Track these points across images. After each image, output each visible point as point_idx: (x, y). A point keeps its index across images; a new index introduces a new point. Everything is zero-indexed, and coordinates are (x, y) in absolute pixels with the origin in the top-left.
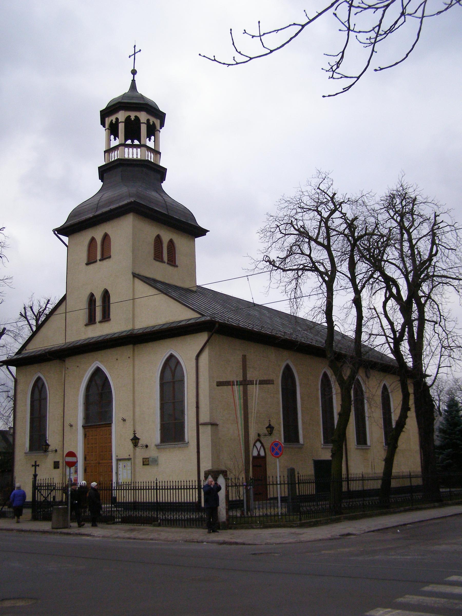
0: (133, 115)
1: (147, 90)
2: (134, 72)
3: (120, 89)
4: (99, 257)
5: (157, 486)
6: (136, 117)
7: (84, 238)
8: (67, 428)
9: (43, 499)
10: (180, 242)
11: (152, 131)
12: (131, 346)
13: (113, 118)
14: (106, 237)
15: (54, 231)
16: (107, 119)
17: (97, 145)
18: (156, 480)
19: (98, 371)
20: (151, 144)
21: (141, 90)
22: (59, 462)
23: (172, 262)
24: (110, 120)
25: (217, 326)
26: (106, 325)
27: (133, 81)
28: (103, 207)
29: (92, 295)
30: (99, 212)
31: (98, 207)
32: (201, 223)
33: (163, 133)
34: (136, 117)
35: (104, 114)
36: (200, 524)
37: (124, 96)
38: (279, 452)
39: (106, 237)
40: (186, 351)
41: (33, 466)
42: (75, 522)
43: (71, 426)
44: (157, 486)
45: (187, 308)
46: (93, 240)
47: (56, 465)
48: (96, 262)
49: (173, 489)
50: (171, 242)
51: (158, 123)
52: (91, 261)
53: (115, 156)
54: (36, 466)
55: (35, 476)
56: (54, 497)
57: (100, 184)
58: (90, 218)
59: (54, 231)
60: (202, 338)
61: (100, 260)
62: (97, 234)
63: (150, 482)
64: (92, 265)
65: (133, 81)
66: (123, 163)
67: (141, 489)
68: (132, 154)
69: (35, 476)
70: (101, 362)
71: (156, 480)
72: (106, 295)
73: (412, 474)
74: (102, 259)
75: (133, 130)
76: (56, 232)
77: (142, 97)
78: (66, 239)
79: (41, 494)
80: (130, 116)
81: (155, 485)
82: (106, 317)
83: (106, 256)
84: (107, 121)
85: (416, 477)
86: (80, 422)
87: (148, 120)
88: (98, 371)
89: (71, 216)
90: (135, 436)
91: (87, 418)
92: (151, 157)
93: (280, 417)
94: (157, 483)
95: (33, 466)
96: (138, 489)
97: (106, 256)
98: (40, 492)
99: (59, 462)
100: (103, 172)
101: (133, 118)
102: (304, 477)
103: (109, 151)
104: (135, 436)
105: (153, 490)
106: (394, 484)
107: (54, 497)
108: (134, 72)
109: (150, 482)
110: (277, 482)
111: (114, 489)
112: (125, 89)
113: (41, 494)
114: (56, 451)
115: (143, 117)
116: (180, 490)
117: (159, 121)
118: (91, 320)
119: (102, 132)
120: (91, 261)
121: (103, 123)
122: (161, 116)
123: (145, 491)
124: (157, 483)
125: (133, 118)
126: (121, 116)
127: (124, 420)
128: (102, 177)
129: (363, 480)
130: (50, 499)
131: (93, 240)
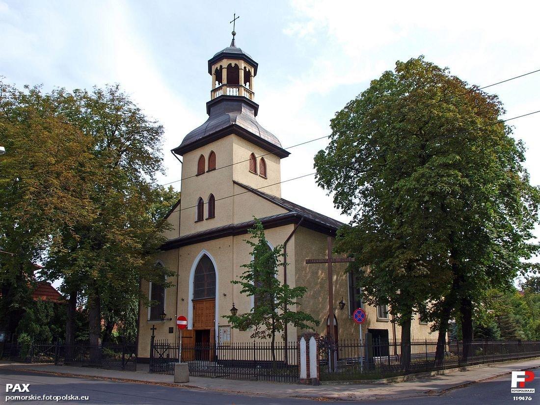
0: (233, 63)
1: (243, 46)
2: (234, 34)
3: (223, 45)
4: (206, 169)
5: (255, 347)
7: (196, 155)
8: (179, 302)
9: (159, 356)
10: (270, 162)
11: (248, 78)
12: (232, 236)
13: (218, 66)
14: (212, 154)
15: (172, 151)
16: (213, 67)
17: (204, 87)
19: (205, 258)
20: (247, 87)
21: (238, 45)
22: (173, 328)
23: (264, 175)
24: (215, 68)
25: (302, 219)
26: (212, 221)
27: (233, 39)
28: (210, 130)
29: (201, 199)
30: (207, 134)
31: (206, 131)
32: (284, 147)
33: (254, 80)
35: (211, 63)
36: (294, 380)
37: (226, 49)
38: (361, 318)
39: (212, 154)
40: (275, 238)
41: (151, 329)
43: (183, 300)
44: (255, 347)
45: (275, 205)
46: (202, 157)
47: (171, 330)
48: (204, 173)
49: (234, 349)
50: (263, 160)
52: (201, 172)
53: (219, 94)
54: (153, 329)
55: (153, 337)
56: (168, 355)
57: (207, 117)
58: (200, 140)
59: (172, 151)
60: (291, 228)
61: (207, 172)
62: (205, 151)
64: (201, 176)
65: (233, 39)
66: (225, 98)
68: (232, 92)
69: (153, 337)
70: (208, 250)
72: (212, 199)
73: (428, 341)
75: (233, 81)
76: (173, 152)
78: (181, 158)
79: (158, 352)
80: (231, 64)
82: (212, 215)
83: (212, 168)
84: (214, 68)
85: (432, 344)
86: (191, 296)
87: (245, 68)
88: (205, 258)
89: (185, 139)
91: (196, 293)
92: (247, 96)
93: (348, 295)
94: (254, 344)
95: (151, 329)
96: (236, 349)
97: (212, 168)
98: (157, 350)
99: (173, 328)
100: (211, 106)
102: (346, 342)
103: (214, 91)
105: (263, 350)
106: (414, 350)
107: (168, 355)
108: (234, 34)
111: (289, 349)
112: (228, 45)
113: (158, 352)
114: (171, 319)
115: (242, 65)
117: (253, 69)
118: (200, 218)
119: (210, 78)
120: (201, 172)
121: (210, 72)
122: (255, 65)
123: (263, 350)
124: (254, 344)
126: (225, 63)
127: (225, 295)
128: (209, 112)
129: (426, 345)
130: (165, 356)
131: (202, 157)
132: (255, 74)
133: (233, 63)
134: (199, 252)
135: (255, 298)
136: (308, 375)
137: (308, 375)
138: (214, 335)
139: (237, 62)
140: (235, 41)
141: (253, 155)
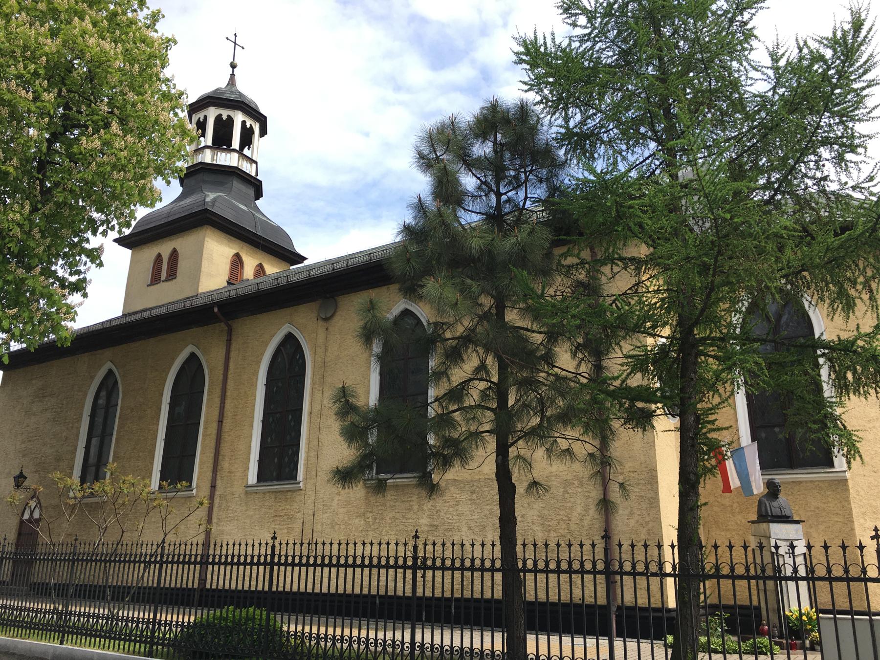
0: (225, 113)
1: (247, 88)
2: (233, 66)
3: (217, 82)
6: (229, 116)
7: (149, 253)
11: (247, 138)
13: (200, 115)
18: (274, 538)
27: (233, 75)
30: (170, 219)
31: (169, 214)
34: (229, 116)
42: (284, 324)
46: (159, 255)
51: (257, 128)
52: (155, 279)
62: (165, 248)
63: (231, 543)
65: (233, 75)
67: (346, 565)
71: (416, 537)
72: (553, 34)
74: (167, 280)
77: (241, 95)
81: (269, 552)
83: (172, 274)
84: (195, 118)
87: (244, 123)
90: (21, 473)
101: (224, 117)
104: (21, 473)
108: (233, 66)
109: (231, 543)
110: (661, 565)
115: (239, 118)
116: (319, 569)
122: (262, 120)
125: (224, 117)
126: (212, 114)
131: (159, 255)
132: (263, 132)
133: (225, 113)
134: (264, 339)
135: (814, 335)
136: (345, 590)
137: (345, 590)
138: (708, 488)
139: (231, 113)
140: (237, 78)
141: (237, 256)
